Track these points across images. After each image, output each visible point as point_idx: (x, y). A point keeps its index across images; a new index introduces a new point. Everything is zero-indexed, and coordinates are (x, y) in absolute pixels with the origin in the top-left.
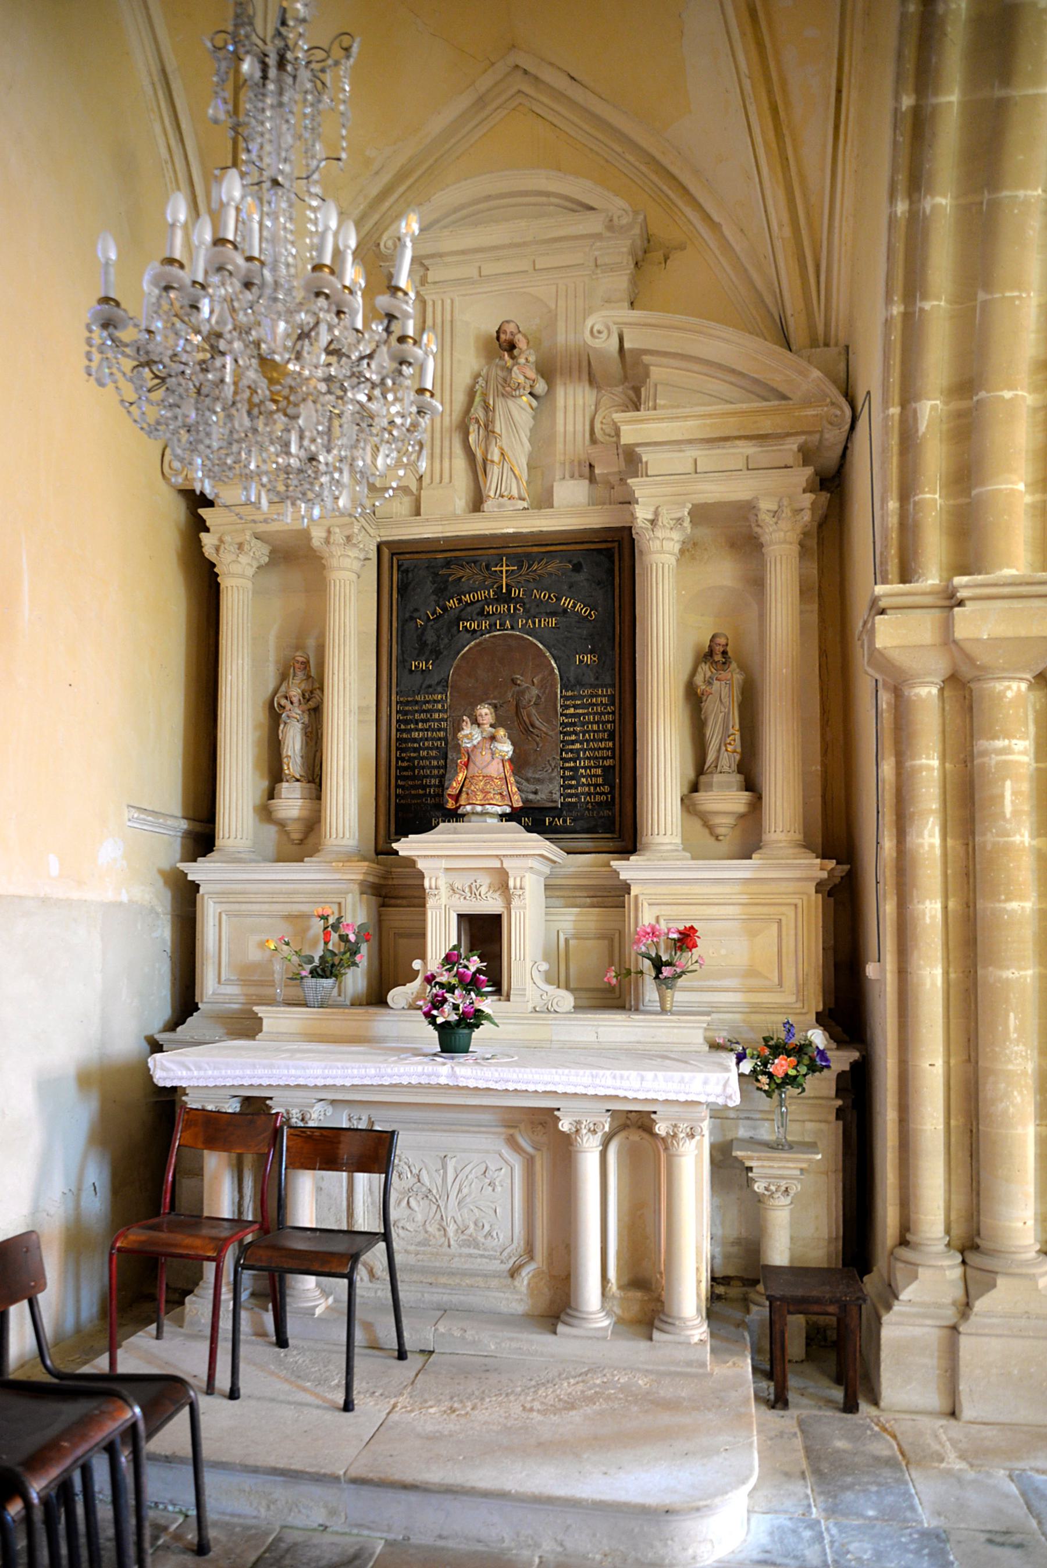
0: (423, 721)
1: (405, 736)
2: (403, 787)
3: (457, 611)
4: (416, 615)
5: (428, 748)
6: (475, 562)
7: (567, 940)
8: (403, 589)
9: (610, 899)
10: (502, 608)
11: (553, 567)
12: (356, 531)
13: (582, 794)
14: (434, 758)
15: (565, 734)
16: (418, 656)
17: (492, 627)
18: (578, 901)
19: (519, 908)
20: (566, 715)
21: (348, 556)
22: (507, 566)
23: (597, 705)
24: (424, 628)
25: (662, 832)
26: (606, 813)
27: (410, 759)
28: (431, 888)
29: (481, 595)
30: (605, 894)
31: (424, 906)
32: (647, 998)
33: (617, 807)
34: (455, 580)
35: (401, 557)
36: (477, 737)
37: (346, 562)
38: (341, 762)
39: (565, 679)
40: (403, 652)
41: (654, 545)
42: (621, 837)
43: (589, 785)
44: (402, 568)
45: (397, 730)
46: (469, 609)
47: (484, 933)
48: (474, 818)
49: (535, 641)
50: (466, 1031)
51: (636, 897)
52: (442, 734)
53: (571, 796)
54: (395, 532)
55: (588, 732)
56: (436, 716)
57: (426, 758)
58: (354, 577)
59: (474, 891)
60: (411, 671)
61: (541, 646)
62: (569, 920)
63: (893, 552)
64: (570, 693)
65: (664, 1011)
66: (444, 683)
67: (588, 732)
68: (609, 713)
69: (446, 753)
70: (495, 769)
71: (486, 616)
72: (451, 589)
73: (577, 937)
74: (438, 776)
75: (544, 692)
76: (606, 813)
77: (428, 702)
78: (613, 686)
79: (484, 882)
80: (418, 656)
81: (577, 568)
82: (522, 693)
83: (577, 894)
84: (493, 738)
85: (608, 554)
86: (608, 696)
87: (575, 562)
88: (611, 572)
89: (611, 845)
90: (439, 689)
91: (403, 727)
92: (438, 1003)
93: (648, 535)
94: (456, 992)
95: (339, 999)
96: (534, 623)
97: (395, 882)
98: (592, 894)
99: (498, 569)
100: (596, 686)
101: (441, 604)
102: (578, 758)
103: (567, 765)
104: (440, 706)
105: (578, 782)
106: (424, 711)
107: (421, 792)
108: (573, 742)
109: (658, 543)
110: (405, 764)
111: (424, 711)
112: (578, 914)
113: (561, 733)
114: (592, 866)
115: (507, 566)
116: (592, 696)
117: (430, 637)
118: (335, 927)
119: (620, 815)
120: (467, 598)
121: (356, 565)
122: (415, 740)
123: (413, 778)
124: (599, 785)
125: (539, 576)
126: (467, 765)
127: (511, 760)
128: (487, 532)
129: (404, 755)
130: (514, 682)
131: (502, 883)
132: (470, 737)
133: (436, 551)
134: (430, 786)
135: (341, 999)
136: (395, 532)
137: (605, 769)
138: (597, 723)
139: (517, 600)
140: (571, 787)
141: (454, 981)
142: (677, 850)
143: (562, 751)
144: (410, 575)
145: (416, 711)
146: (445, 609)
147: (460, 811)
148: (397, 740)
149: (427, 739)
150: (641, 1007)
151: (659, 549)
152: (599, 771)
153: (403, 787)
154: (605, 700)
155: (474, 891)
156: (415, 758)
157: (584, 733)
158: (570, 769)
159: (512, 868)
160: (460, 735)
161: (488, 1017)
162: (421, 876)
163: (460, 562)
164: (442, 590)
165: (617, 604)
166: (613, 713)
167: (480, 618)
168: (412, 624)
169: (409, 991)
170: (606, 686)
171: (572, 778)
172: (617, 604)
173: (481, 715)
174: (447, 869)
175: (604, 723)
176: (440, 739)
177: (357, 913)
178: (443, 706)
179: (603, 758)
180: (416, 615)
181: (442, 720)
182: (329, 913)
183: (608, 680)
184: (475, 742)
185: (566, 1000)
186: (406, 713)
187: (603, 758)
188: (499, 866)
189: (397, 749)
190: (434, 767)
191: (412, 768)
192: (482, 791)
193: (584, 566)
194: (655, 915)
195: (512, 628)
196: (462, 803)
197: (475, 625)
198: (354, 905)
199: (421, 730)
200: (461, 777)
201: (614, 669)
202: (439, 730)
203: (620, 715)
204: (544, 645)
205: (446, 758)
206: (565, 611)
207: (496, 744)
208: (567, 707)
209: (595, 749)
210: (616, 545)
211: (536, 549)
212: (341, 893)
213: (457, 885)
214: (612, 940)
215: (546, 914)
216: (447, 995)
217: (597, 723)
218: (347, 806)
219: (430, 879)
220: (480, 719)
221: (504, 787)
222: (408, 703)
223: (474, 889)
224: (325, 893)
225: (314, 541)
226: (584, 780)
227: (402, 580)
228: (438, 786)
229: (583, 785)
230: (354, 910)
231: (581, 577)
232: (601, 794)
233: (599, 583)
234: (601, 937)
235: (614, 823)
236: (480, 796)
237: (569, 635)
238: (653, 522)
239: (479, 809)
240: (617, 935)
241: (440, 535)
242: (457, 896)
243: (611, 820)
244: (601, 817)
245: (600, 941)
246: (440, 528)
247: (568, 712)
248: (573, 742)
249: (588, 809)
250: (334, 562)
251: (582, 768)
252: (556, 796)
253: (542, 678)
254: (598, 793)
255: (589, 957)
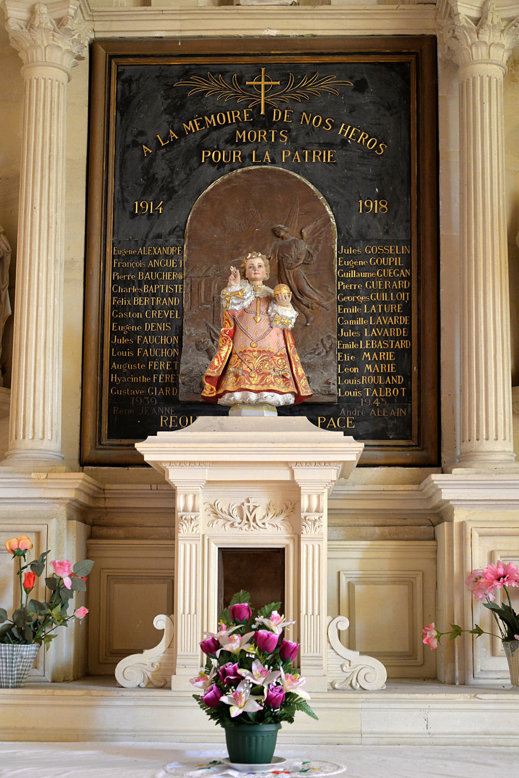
0: (149, 282)
1: (123, 302)
2: (119, 372)
3: (198, 136)
4: (140, 140)
5: (155, 320)
6: (223, 73)
7: (350, 586)
8: (125, 105)
9: (407, 529)
10: (261, 135)
11: (328, 84)
12: (72, 12)
13: (367, 386)
14: (164, 333)
15: (344, 304)
16: (143, 194)
17: (246, 159)
18: (364, 531)
19: (313, 539)
20: (344, 280)
21: (59, 47)
22: (267, 80)
23: (387, 267)
24: (152, 158)
25: (492, 436)
26: (400, 412)
27: (130, 335)
28: (185, 510)
29: (231, 117)
30: (398, 522)
31: (172, 537)
32: (478, 667)
33: (415, 404)
34: (196, 96)
35: (124, 61)
36: (249, 297)
37: (55, 56)
38: (42, 332)
39: (344, 232)
40: (122, 190)
41: (479, 53)
42: (420, 445)
43: (376, 374)
44: (123, 77)
45: (113, 294)
46: (215, 135)
47: (254, 576)
48: (245, 411)
49: (304, 180)
50: (271, 728)
51: (462, 525)
52: (174, 301)
53: (351, 388)
54: (115, 26)
55: (375, 303)
56: (167, 276)
57: (153, 334)
58: (63, 77)
59: (246, 515)
60: (133, 215)
61: (312, 187)
62: (357, 556)
63: (456, 205)
64: (350, 251)
65: (464, 683)
66: (179, 232)
67: (375, 303)
68: (402, 278)
69: (181, 328)
70: (274, 342)
71: (238, 145)
72: (191, 107)
73: (365, 580)
74: (168, 359)
75: (316, 248)
76: (400, 412)
77: (156, 257)
78: (409, 243)
79: (261, 500)
80: (143, 194)
81: (361, 87)
82: (288, 247)
83: (361, 522)
84: (270, 300)
85: (402, 70)
86: (402, 256)
87: (358, 78)
88: (405, 94)
89: (408, 455)
90: (172, 240)
91: (120, 290)
92: (225, 682)
93: (470, 38)
94: (254, 667)
95: (35, 672)
96: (303, 156)
97: (109, 504)
98: (380, 521)
99: (254, 83)
100: (386, 243)
101: (176, 125)
102: (362, 337)
103: (347, 346)
104: (172, 263)
105: (361, 369)
106: (150, 269)
107: (145, 379)
108: (354, 316)
109: (484, 49)
110: (124, 341)
111: (150, 269)
112: (367, 550)
113: (339, 303)
114: (374, 484)
115: (267, 80)
116: (380, 255)
117: (161, 170)
118: (38, 566)
119: (419, 416)
120: (212, 120)
121: (68, 61)
122: (137, 309)
123: (135, 360)
124: (390, 375)
125: (309, 94)
126: (233, 335)
127: (293, 331)
128: (241, 33)
129: (121, 328)
130: (275, 233)
131: (289, 501)
132: (239, 296)
133: (171, 56)
134: (157, 372)
135: (39, 672)
136: (115, 26)
137: (397, 353)
138: (387, 291)
139: (281, 126)
140: (351, 376)
141: (252, 650)
142: (511, 461)
143: (340, 327)
144: (134, 86)
145: (140, 269)
146: (181, 133)
147: (221, 401)
148: (113, 307)
149: (154, 308)
150: (472, 681)
151: (485, 57)
152: (390, 356)
153: (119, 372)
154: (398, 261)
155: (246, 515)
156: (137, 333)
157: (370, 304)
158: (352, 352)
159: (305, 481)
160: (224, 291)
161: (302, 705)
162: (171, 493)
163: (203, 73)
164: (178, 108)
165: (414, 136)
166: (409, 278)
167: (229, 147)
168: (136, 152)
169: (148, 662)
170: (398, 242)
171: (353, 364)
172: (414, 136)
173: (252, 267)
174: (208, 482)
175: (395, 291)
176: (172, 308)
177: (63, 549)
178: (177, 263)
179: (395, 339)
180: (140, 140)
181: (176, 282)
182: (28, 546)
183: (402, 235)
184: (246, 304)
185: (376, 672)
186: (125, 271)
187: (395, 339)
188: (288, 478)
189: (113, 320)
190: (163, 346)
191: (134, 347)
192: (258, 371)
193: (370, 85)
194: (487, 551)
195: (273, 162)
196: (229, 388)
197: (222, 156)
198: (59, 535)
199: (147, 295)
200: (225, 351)
201: (409, 221)
202: (171, 295)
203: (419, 281)
204: (316, 186)
205: (180, 335)
206: (344, 142)
207: (276, 307)
208: (347, 269)
209: (384, 326)
210: (413, 58)
211: (306, 59)
212: (41, 518)
213: (222, 505)
214: (412, 586)
215: (328, 548)
216: (242, 672)
217: (387, 291)
218: (49, 394)
219: (186, 496)
220: (250, 272)
221: (287, 366)
222: (128, 258)
223: (246, 512)
224: (16, 518)
225: (10, 22)
226: (369, 367)
227: (123, 95)
228: (169, 372)
229: (368, 373)
230: (59, 543)
231: (365, 99)
232: (392, 386)
233: (389, 108)
234: (397, 581)
235: (410, 426)
236: (256, 379)
237: (350, 174)
238: (477, 21)
239: (253, 397)
240: (419, 578)
241: (177, 34)
242: (221, 522)
243: (407, 422)
244: (392, 418)
245: (396, 587)
246: (177, 25)
247: (348, 275)
248: (354, 316)
249: (375, 407)
250: (38, 55)
251: (367, 351)
252: (333, 388)
253: (317, 225)
254: (388, 385)
255: (385, 606)
